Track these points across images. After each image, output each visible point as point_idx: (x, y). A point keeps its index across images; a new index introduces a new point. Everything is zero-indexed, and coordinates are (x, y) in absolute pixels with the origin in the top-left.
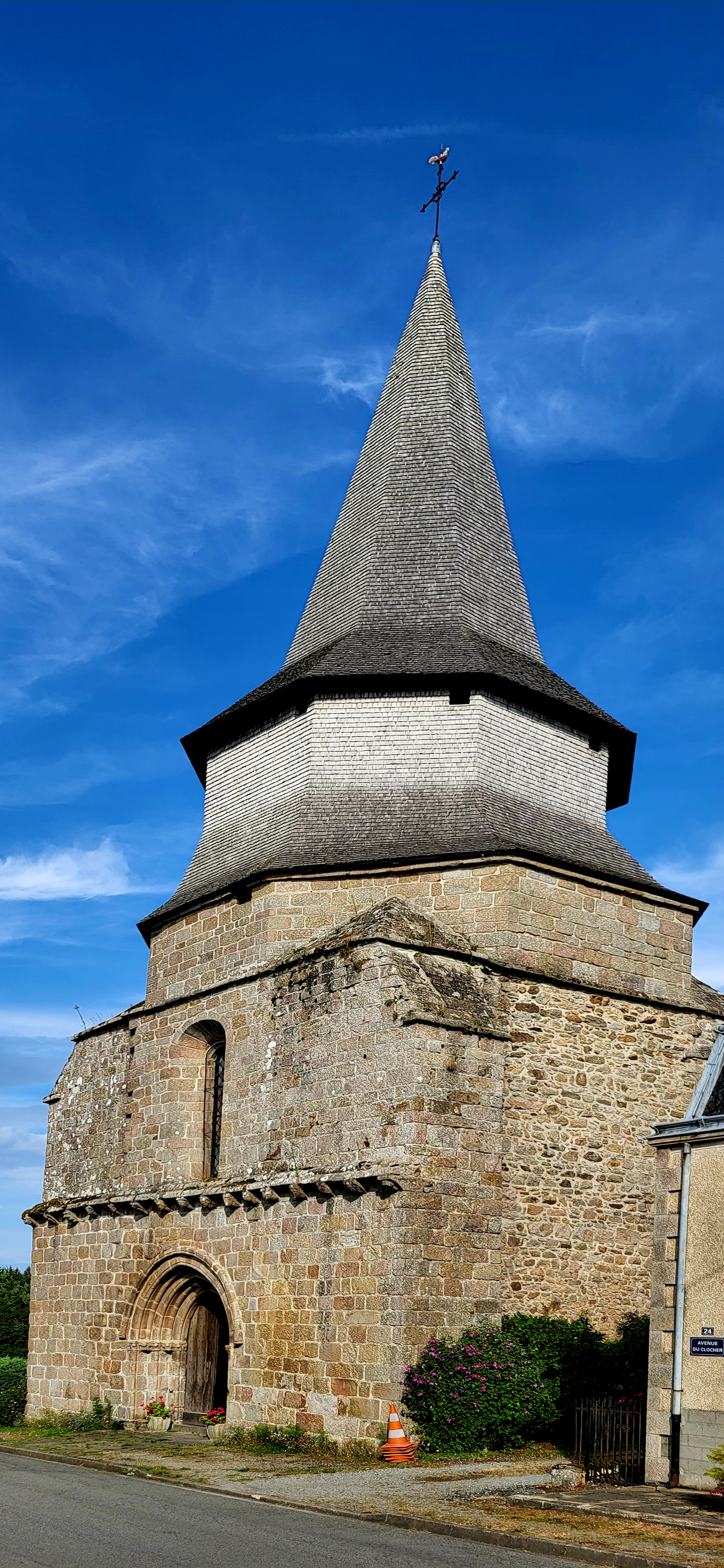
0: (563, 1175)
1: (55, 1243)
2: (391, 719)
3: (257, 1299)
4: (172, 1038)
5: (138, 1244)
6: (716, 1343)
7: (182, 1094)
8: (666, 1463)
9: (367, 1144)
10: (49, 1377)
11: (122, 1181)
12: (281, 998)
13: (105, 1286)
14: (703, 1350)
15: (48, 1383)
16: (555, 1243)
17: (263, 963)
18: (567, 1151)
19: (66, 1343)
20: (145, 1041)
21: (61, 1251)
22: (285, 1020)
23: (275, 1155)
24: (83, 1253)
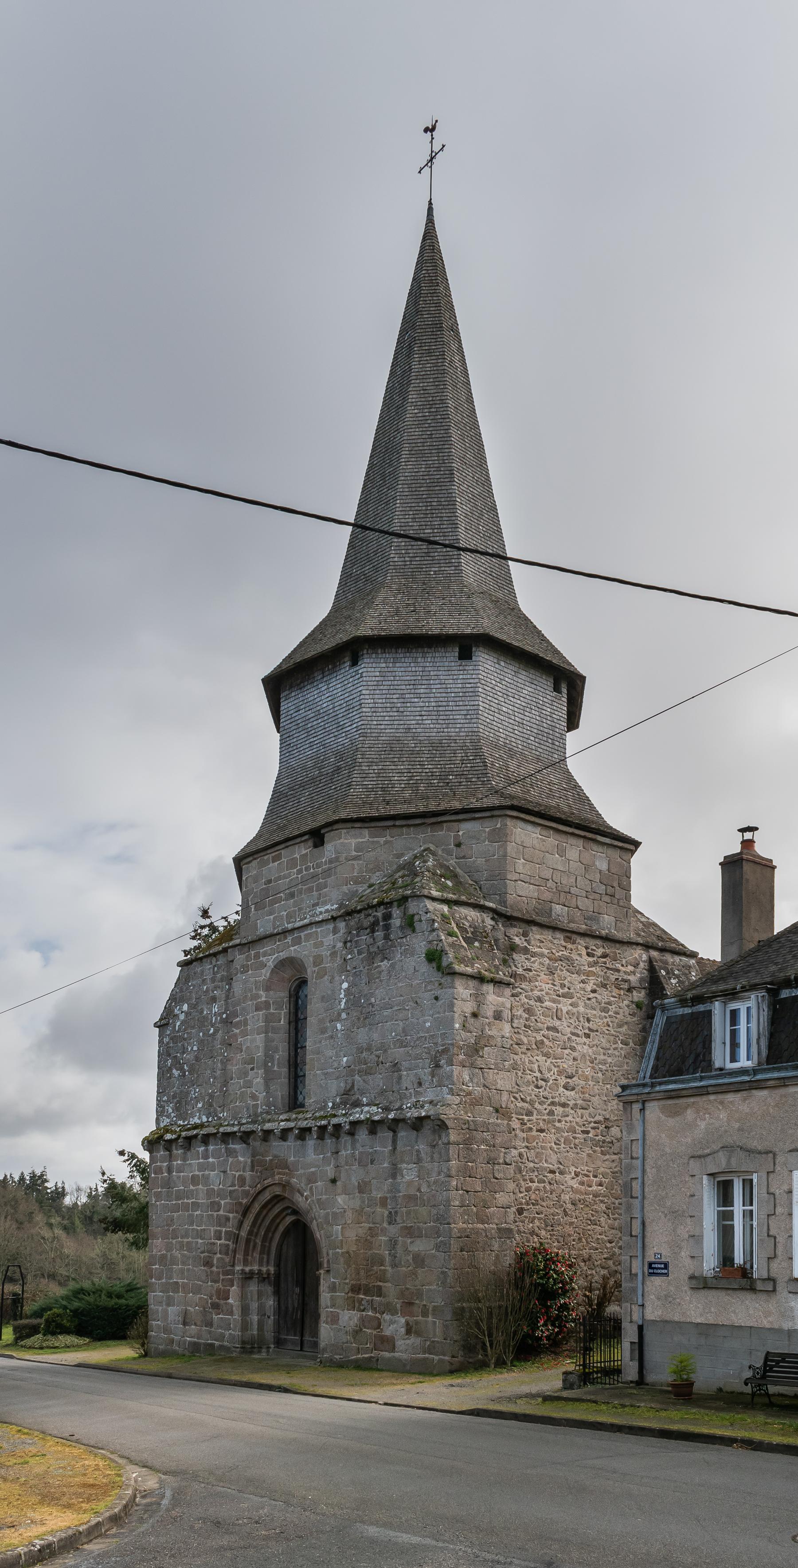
0: (549, 1105)
1: (170, 1171)
3: (340, 1227)
4: (263, 971)
5: (241, 1173)
6: (663, 1266)
7: (272, 1027)
8: (635, 1364)
9: (420, 1084)
10: (168, 1305)
12: (351, 941)
13: (215, 1214)
14: (655, 1271)
15: (167, 1310)
16: (545, 1169)
17: (336, 906)
18: (551, 1082)
19: (182, 1271)
20: (242, 973)
21: (175, 1178)
23: (350, 1090)
24: (195, 1180)
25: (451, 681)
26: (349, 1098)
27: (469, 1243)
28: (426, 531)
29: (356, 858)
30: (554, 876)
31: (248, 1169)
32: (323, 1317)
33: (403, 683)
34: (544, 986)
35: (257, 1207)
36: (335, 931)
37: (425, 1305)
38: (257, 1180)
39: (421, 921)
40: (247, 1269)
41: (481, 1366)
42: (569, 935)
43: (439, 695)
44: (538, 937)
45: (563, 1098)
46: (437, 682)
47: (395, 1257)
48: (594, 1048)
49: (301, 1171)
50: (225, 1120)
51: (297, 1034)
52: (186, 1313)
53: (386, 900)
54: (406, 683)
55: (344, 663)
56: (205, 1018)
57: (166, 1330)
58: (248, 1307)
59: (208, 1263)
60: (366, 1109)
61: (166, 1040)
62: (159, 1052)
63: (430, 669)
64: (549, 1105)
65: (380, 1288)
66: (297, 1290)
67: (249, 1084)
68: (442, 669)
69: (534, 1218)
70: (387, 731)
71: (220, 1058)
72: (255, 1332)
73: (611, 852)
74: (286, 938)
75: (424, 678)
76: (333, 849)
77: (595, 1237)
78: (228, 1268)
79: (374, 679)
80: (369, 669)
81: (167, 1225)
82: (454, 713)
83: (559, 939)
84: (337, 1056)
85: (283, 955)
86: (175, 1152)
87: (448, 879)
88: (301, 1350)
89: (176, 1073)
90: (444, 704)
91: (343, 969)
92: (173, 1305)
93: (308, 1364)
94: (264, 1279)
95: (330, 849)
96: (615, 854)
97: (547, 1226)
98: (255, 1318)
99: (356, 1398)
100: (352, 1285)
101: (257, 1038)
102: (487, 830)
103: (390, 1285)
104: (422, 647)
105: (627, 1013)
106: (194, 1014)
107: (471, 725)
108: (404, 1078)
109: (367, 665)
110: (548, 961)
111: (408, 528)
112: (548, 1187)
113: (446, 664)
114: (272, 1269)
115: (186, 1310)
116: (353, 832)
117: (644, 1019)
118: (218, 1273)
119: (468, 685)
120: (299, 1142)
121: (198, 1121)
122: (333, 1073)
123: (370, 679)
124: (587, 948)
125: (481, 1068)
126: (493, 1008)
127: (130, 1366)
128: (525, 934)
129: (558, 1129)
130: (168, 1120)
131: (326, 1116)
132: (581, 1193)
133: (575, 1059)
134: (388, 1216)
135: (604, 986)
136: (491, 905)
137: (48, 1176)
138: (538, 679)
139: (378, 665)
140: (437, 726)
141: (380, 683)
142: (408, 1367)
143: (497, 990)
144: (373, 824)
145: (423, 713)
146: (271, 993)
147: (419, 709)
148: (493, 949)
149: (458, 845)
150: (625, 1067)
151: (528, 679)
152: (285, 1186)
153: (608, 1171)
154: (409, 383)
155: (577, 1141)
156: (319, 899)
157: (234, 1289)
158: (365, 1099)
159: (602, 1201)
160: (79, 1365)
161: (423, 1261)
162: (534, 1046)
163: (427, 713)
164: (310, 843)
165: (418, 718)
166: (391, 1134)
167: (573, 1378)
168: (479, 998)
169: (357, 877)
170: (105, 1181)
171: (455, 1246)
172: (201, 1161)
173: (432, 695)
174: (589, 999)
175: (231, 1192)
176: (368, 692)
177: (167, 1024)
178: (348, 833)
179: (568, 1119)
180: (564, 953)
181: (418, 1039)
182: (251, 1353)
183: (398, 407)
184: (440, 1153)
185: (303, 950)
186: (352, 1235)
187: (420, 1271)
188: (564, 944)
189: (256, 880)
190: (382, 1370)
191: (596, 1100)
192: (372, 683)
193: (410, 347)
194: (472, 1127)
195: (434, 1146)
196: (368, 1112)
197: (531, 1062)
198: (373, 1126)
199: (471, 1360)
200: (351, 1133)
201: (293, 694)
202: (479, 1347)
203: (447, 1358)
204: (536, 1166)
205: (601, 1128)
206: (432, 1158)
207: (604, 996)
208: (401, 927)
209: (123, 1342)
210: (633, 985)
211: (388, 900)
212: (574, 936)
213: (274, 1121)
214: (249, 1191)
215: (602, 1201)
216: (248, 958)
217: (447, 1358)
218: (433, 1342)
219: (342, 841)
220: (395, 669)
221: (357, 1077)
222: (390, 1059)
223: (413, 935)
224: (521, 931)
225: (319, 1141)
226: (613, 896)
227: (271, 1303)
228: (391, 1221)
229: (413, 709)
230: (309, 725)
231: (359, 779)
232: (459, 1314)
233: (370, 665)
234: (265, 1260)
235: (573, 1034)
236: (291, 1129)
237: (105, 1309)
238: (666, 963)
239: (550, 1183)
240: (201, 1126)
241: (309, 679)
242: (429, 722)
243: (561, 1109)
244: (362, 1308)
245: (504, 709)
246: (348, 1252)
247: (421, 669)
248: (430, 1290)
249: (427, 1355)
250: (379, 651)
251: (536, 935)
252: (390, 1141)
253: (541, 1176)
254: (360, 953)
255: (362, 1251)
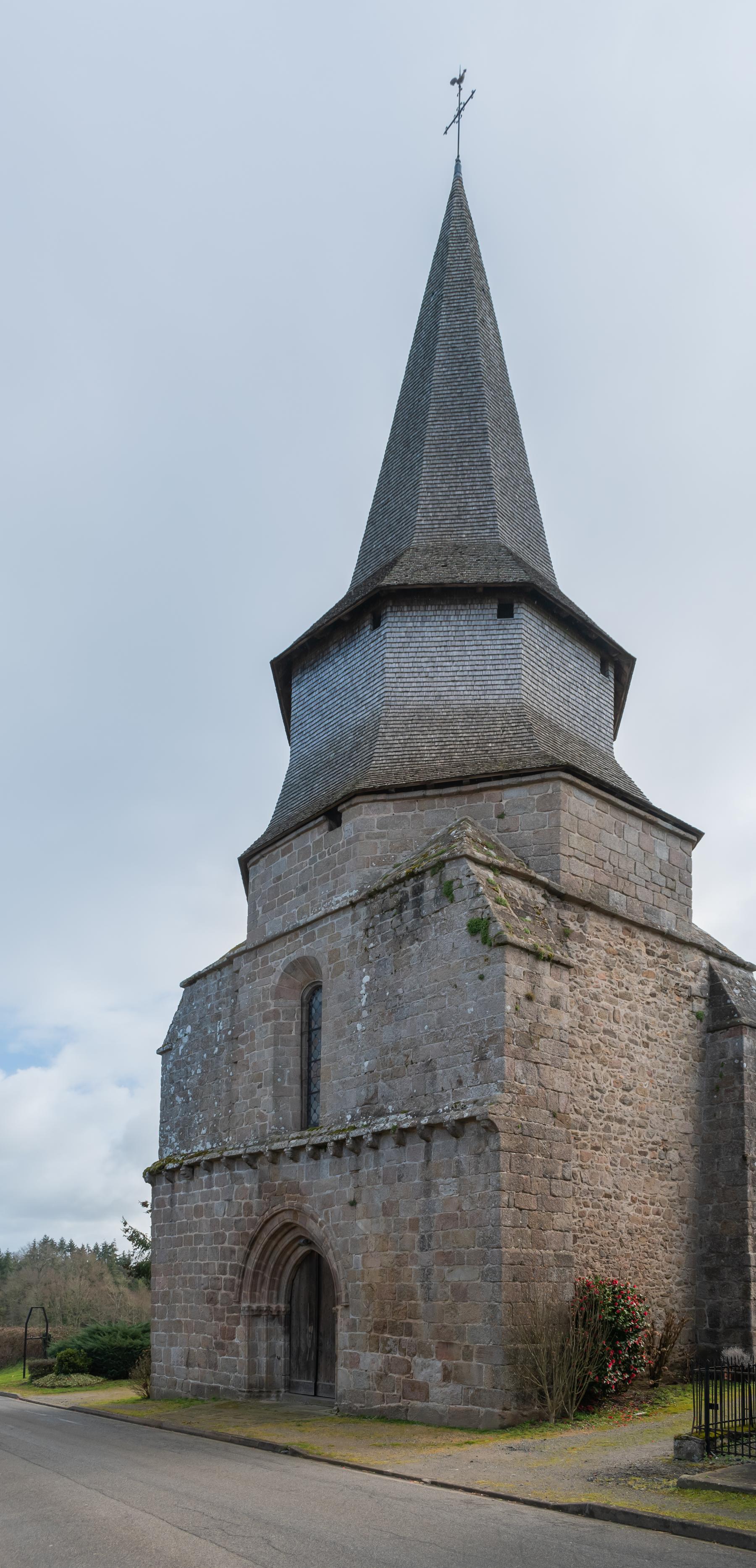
0: (605, 1119)
2: (450, 633)
3: (360, 1256)
4: (272, 977)
5: (248, 1200)
9: (460, 1083)
10: (171, 1345)
11: (231, 1134)
12: (373, 927)
13: (219, 1246)
15: (170, 1351)
16: (600, 1192)
17: (355, 892)
19: (185, 1309)
20: (249, 982)
21: (177, 1210)
22: (377, 952)
23: (372, 1098)
24: (198, 1211)
25: (489, 642)
26: (371, 1107)
27: (524, 1272)
28: (456, 493)
29: (381, 836)
30: (612, 857)
31: (255, 1195)
32: (340, 1360)
33: (433, 644)
34: (600, 982)
35: (265, 1237)
36: (354, 919)
37: (467, 1347)
38: (265, 1207)
39: (461, 887)
40: (255, 1306)
41: (538, 1421)
42: (628, 926)
43: (475, 658)
44: (595, 924)
45: (619, 1113)
46: (473, 643)
47: (429, 1289)
48: (653, 1060)
49: (315, 1195)
50: (230, 1144)
51: (310, 1046)
52: (189, 1353)
53: (417, 870)
54: (437, 644)
55: (364, 627)
56: (209, 1038)
57: (169, 1371)
58: (253, 1348)
59: (212, 1300)
60: (393, 1117)
61: (169, 1066)
62: (162, 1079)
63: (464, 628)
64: (605, 1119)
65: (409, 1326)
66: (311, 1329)
67: (256, 1104)
68: (478, 628)
69: (589, 1247)
70: (414, 699)
71: (225, 1079)
72: (264, 1375)
73: (671, 840)
74: (297, 936)
75: (457, 639)
76: (352, 828)
77: (652, 1271)
78: (234, 1305)
79: (399, 640)
80: (394, 630)
81: (170, 1260)
82: (492, 678)
83: (618, 929)
84: (357, 1060)
85: (294, 956)
86: (178, 1182)
87: (491, 849)
88: (316, 1395)
89: (179, 1099)
90: (481, 668)
91: (364, 961)
92: (176, 1345)
93: (322, 1412)
94: (274, 1317)
95: (347, 828)
96: (676, 844)
97: (602, 1257)
98: (264, 1360)
99: (390, 1470)
100: (376, 1322)
101: (266, 1052)
102: (536, 797)
103: (423, 1322)
104: (455, 604)
105: (687, 1024)
106: (197, 1035)
107: (512, 692)
108: (439, 1077)
109: (390, 625)
110: (605, 954)
111: (436, 490)
112: (603, 1213)
113: (484, 623)
114: (282, 1306)
115: (189, 1350)
116: (375, 806)
117: (704, 1033)
118: (223, 1311)
119: (508, 647)
120: (313, 1162)
121: (202, 1149)
122: (352, 1080)
123: (395, 640)
124: (646, 944)
125: (536, 1063)
126: (550, 993)
127: (121, 1411)
128: (580, 920)
129: (613, 1147)
130: (171, 1151)
131: (344, 1130)
132: (638, 1222)
133: (632, 1070)
134: (420, 1242)
135: (664, 990)
136: (543, 878)
137: (117, 1246)
138: (584, 654)
139: (403, 625)
140: (472, 693)
141: (406, 645)
142: (446, 1420)
143: (554, 972)
144: (399, 796)
145: (456, 678)
146: (281, 1001)
147: (451, 674)
148: (547, 928)
149: (501, 816)
150: (684, 1084)
151: (574, 653)
152: (296, 1211)
153: (666, 1199)
154: (436, 341)
155: (634, 1163)
156: (335, 887)
157: (240, 1328)
158: (390, 1107)
159: (659, 1232)
160: (72, 1409)
161: (465, 1293)
162: (589, 1051)
163: (461, 679)
164: (325, 826)
165: (451, 684)
166: (423, 1144)
167: (689, 1446)
168: (533, 977)
169: (380, 858)
170: (127, 1231)
171: (506, 1274)
172: (204, 1190)
173: (467, 658)
174: (648, 1003)
175: (236, 1222)
176: (392, 655)
177: (170, 1050)
178: (369, 807)
179: (626, 1137)
180: (623, 947)
181: (458, 1029)
182: (260, 1397)
183: (424, 370)
184: (488, 1163)
185: (317, 947)
186: (374, 1264)
187: (460, 1305)
188: (623, 936)
189: (263, 880)
190: (413, 1423)
191: (653, 1117)
192: (397, 645)
193: (437, 306)
194: (526, 1132)
195: (479, 1154)
196: (396, 1120)
197: (585, 1068)
198: (402, 1135)
199: (525, 1413)
200: (374, 1147)
201: (306, 677)
202: (535, 1395)
203: (497, 1410)
204: (591, 1188)
205: (659, 1150)
206: (477, 1169)
207: (663, 1001)
208: (436, 899)
209: (125, 1382)
210: (694, 992)
211: (420, 869)
212: (634, 929)
213: (284, 1140)
214: (256, 1220)
215: (659, 1232)
216: (255, 965)
217: (497, 1410)
218: (478, 1390)
219: (362, 816)
220: (424, 629)
221: (381, 1083)
222: (422, 1058)
223: (451, 906)
224: (576, 915)
225: (336, 1159)
226: (673, 890)
227: (281, 1343)
228: (424, 1246)
229: (444, 674)
230: (324, 706)
231: (382, 750)
232: (512, 1358)
233: (395, 624)
234: (275, 1296)
235: (631, 1041)
236: (303, 1147)
237: (120, 1349)
238: (727, 973)
239: (606, 1209)
240: (205, 1152)
241: (323, 656)
242: (464, 688)
243: (618, 1125)
244: (387, 1349)
245: (548, 680)
246: (370, 1285)
247: (453, 628)
248: (475, 1328)
249: (470, 1406)
250: (405, 609)
251: (593, 921)
252: (422, 1153)
253: (596, 1201)
254: (384, 939)
255: (387, 1283)
